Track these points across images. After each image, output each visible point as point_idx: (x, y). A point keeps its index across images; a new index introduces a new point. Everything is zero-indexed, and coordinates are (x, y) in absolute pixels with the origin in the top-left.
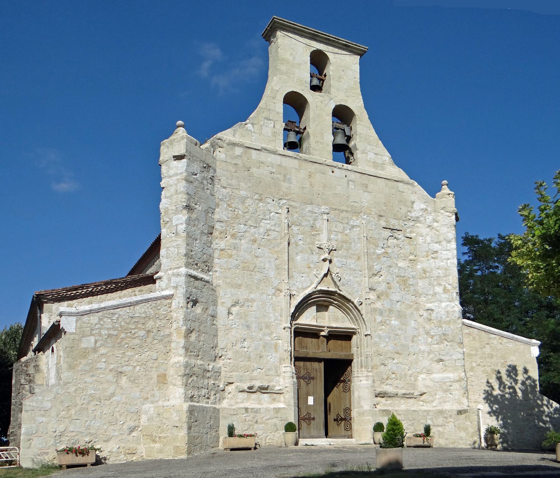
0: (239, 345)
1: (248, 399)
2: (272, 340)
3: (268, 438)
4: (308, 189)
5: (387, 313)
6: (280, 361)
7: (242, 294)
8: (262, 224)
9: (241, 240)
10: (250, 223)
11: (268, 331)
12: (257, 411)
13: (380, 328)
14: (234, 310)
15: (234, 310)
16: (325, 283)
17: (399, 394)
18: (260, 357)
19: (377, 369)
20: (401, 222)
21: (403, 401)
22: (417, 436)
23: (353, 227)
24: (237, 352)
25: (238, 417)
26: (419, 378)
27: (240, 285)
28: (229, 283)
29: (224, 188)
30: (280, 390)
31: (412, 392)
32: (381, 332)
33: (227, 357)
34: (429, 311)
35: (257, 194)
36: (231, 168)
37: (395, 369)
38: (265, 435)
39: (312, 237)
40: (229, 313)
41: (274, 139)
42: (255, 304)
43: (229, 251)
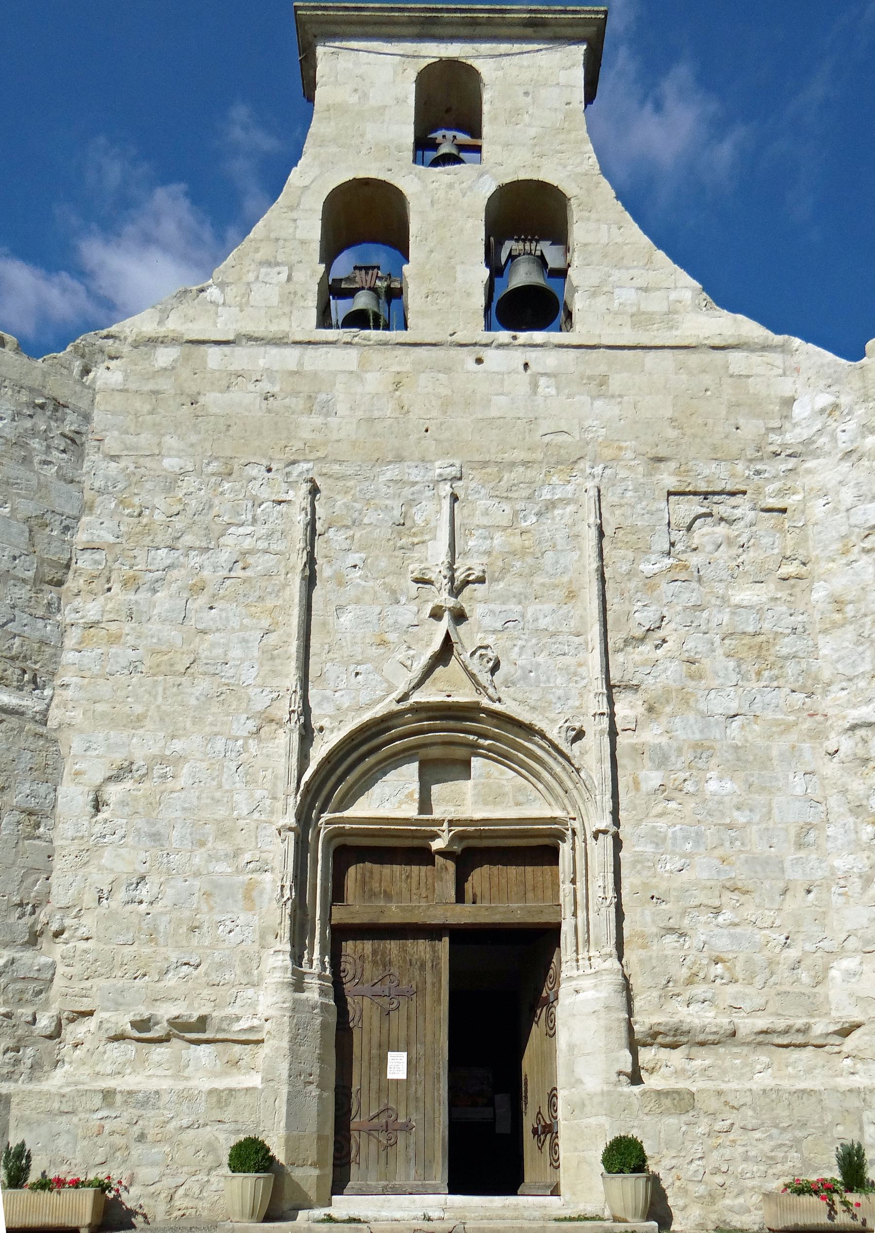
0: (122, 895)
1: (140, 1063)
2: (238, 871)
3: (181, 1191)
4: (389, 422)
5: (688, 755)
6: (262, 937)
7: (143, 746)
8: (226, 540)
9: (155, 591)
10: (188, 539)
11: (223, 847)
12: (147, 1100)
13: (659, 809)
14: (113, 793)
15: (113, 793)
16: (441, 686)
17: (742, 1032)
18: (193, 929)
19: (644, 947)
20: (740, 467)
21: (762, 1058)
22: (801, 1189)
23: (552, 505)
24: (111, 915)
25: (75, 1119)
26: (833, 973)
27: (140, 718)
28: (103, 715)
29: (114, 458)
30: (252, 1029)
31: (799, 1023)
32: (661, 824)
33: (79, 934)
34: (862, 732)
35: (217, 458)
36: (138, 404)
37: (722, 944)
38: (169, 1182)
39: (399, 553)
40: (97, 805)
41: (287, 310)
42: (186, 770)
43: (113, 627)
